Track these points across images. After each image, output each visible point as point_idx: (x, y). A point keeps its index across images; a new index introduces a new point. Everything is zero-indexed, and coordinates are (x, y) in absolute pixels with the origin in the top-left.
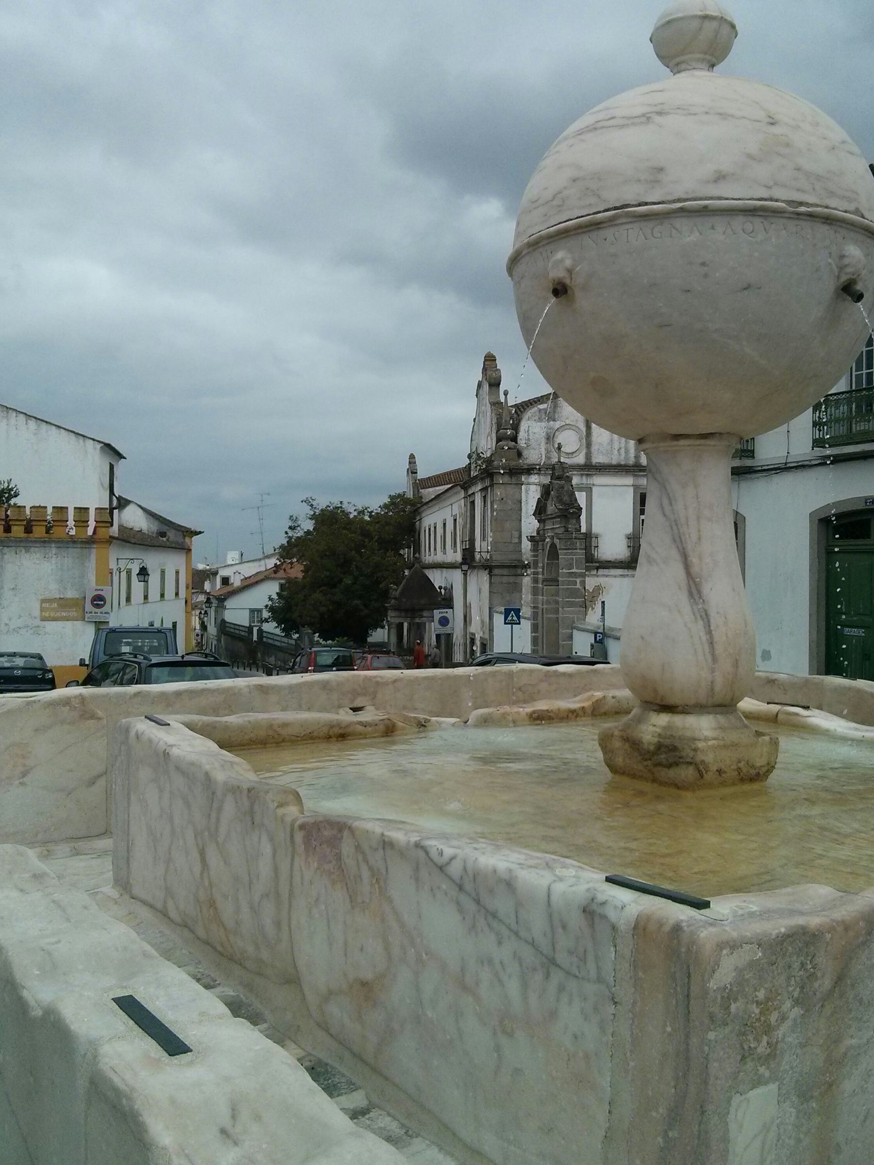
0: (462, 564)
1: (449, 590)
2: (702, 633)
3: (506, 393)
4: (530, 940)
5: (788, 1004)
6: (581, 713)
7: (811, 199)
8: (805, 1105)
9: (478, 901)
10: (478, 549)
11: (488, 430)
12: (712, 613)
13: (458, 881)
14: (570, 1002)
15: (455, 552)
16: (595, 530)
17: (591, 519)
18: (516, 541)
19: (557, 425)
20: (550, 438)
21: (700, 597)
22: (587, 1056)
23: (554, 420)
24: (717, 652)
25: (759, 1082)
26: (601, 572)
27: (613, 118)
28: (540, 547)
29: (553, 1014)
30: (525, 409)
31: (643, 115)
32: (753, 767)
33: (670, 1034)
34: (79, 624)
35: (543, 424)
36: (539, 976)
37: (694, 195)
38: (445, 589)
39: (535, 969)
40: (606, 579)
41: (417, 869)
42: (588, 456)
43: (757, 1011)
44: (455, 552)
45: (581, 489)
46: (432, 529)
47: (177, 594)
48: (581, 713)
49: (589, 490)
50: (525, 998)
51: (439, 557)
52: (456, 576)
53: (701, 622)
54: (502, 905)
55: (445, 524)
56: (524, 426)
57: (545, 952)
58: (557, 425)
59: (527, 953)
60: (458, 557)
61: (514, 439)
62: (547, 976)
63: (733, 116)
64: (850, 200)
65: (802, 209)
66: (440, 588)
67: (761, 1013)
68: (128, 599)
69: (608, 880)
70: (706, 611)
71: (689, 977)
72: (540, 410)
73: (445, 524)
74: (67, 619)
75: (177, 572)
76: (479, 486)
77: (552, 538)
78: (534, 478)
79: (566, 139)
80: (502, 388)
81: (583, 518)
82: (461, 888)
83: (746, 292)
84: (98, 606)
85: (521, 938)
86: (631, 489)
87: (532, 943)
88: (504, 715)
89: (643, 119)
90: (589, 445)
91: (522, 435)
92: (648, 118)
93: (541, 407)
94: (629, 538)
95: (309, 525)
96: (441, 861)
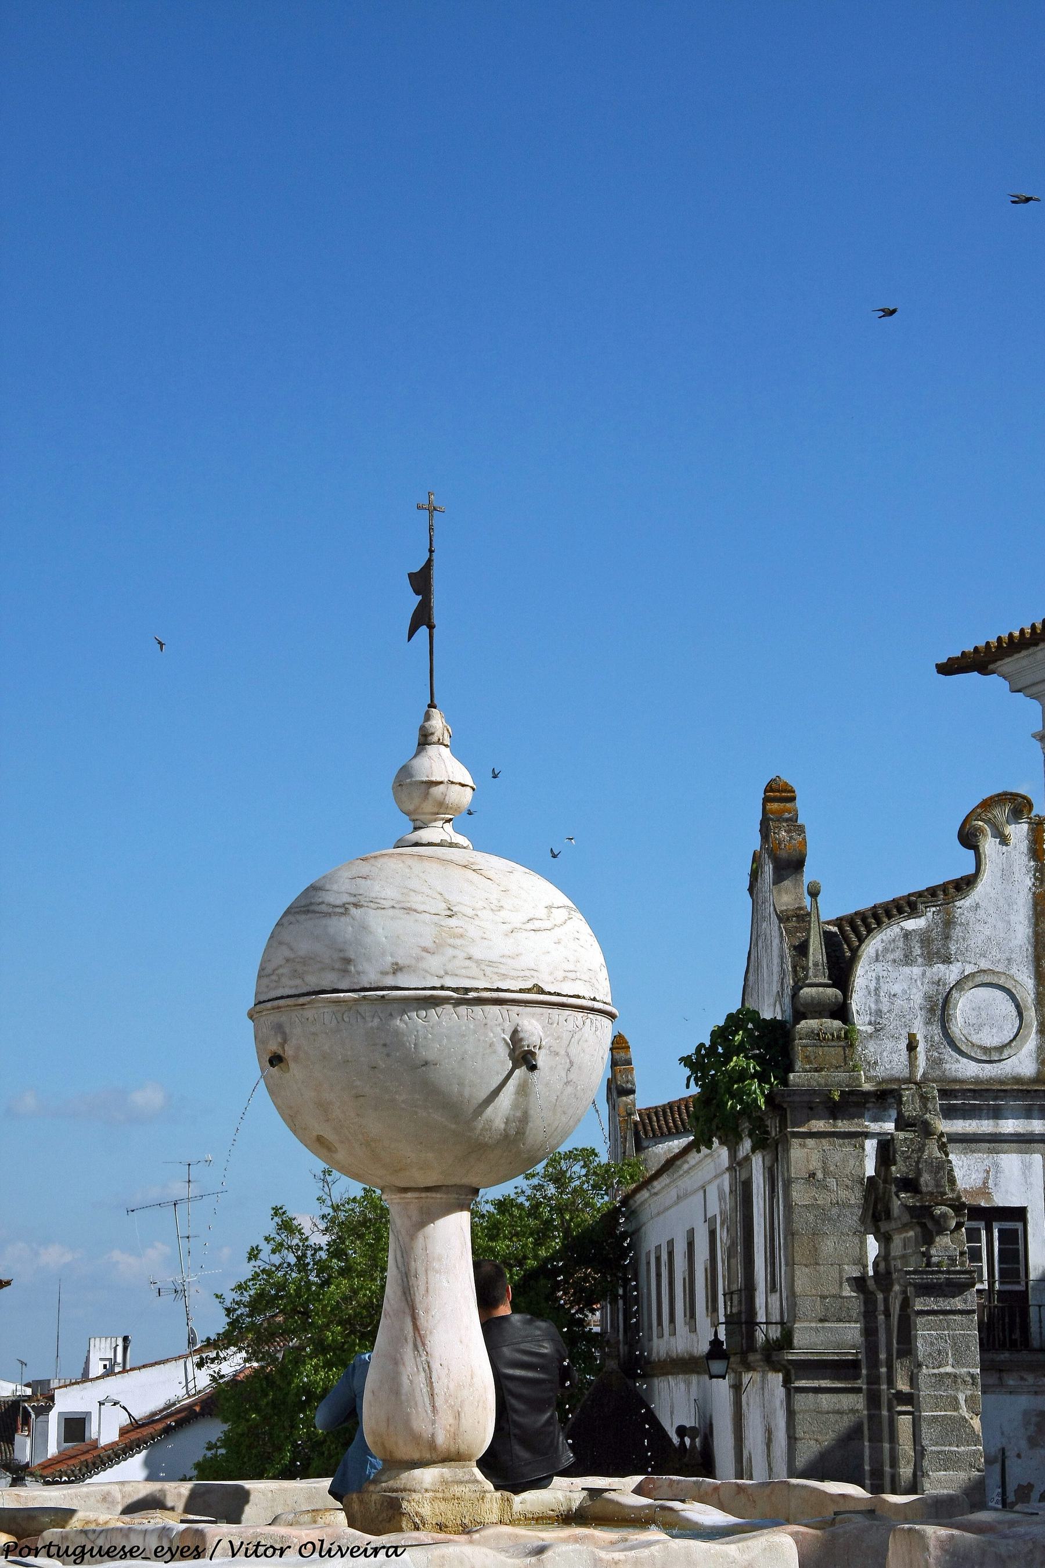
1: (706, 1432)
3: (814, 893)
7: (481, 985)
17: (710, 1241)
19: (952, 973)
21: (424, 1349)
23: (947, 960)
30: (870, 931)
35: (916, 971)
37: (376, 985)
46: (664, 1257)
53: (423, 1374)
56: (863, 976)
58: (952, 973)
61: (841, 1012)
63: (415, 911)
64: (525, 978)
65: (472, 995)
66: (681, 1431)
70: (428, 1363)
72: (907, 935)
80: (809, 874)
89: (342, 910)
91: (858, 1002)
93: (911, 924)
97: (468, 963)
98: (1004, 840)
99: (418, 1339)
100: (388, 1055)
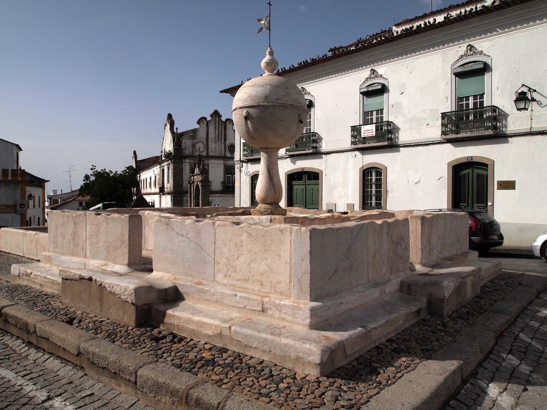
3: (177, 129)
10: (166, 186)
11: (170, 142)
15: (156, 188)
19: (196, 141)
20: (193, 146)
34: (14, 215)
42: (207, 153)
44: (156, 188)
47: (39, 206)
49: (208, 166)
51: (149, 191)
52: (157, 197)
56: (184, 141)
58: (196, 141)
60: (157, 190)
68: (34, 206)
74: (9, 213)
75: (39, 197)
76: (166, 163)
77: (484, 334)
78: (188, 161)
84: (22, 208)
90: (208, 149)
95: (93, 178)
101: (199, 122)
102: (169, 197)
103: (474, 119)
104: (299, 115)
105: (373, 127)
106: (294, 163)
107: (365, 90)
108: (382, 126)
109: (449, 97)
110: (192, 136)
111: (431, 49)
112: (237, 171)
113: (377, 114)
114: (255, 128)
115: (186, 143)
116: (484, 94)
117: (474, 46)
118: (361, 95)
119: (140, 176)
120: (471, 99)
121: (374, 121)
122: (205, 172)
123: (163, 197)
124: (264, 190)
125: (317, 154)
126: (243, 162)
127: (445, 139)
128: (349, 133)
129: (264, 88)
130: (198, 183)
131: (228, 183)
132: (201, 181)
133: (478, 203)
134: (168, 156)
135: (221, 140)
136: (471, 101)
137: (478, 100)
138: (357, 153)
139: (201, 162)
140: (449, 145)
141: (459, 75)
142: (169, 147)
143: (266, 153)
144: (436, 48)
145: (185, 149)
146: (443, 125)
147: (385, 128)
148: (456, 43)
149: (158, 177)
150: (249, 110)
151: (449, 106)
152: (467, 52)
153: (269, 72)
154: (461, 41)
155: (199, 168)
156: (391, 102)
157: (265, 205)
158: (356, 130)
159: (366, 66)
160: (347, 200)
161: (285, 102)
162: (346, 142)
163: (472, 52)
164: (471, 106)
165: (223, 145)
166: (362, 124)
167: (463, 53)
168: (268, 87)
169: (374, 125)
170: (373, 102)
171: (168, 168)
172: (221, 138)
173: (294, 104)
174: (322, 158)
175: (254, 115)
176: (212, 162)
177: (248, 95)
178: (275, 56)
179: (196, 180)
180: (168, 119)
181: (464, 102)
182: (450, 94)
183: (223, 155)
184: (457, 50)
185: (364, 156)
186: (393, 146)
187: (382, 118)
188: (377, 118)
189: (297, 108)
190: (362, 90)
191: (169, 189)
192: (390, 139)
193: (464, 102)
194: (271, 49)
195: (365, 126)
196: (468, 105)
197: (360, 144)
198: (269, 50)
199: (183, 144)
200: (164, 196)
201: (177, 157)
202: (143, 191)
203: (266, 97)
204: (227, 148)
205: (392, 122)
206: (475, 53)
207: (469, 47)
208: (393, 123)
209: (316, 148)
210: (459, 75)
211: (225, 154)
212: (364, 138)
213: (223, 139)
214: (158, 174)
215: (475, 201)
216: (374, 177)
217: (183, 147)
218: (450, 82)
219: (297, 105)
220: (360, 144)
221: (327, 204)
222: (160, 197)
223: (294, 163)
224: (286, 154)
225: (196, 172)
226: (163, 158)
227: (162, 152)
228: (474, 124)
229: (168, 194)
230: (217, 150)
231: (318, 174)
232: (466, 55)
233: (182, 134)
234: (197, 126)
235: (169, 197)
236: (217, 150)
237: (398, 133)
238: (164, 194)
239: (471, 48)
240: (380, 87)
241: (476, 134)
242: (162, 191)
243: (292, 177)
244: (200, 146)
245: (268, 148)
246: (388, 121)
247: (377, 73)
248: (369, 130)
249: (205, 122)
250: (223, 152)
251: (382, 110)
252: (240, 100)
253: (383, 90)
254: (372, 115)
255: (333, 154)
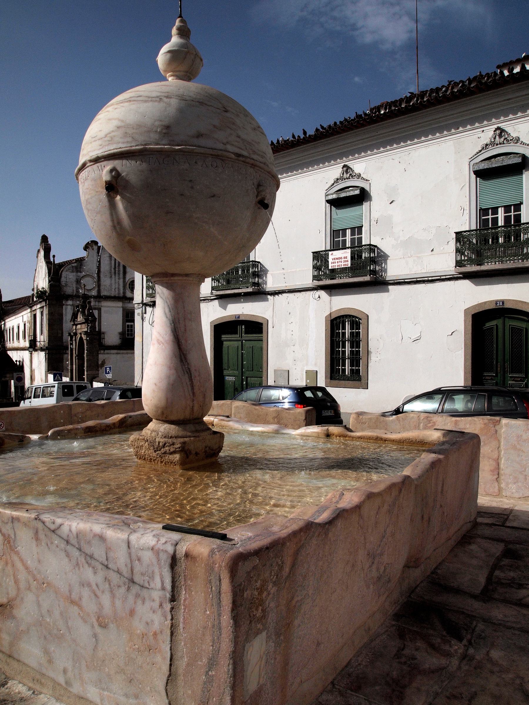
0: (29, 348)
2: (188, 380)
3: (54, 256)
4: (116, 570)
5: (271, 585)
6: (113, 427)
8: (278, 639)
9: (80, 549)
10: (38, 339)
11: (44, 276)
12: (193, 371)
13: (66, 538)
14: (143, 603)
15: (25, 341)
16: (103, 330)
18: (60, 335)
20: (78, 282)
21: (186, 361)
22: (155, 634)
23: (81, 272)
24: (195, 391)
25: (258, 633)
26: (106, 351)
27: (140, 96)
28: (74, 339)
29: (132, 613)
31: (157, 97)
32: (212, 450)
33: (209, 615)
35: (74, 274)
36: (123, 590)
38: (19, 361)
39: (119, 586)
40: (109, 355)
41: (37, 532)
42: (99, 291)
43: (257, 593)
44: (25, 341)
45: (95, 309)
48: (113, 427)
49: (99, 310)
50: (113, 603)
51: (16, 344)
53: (187, 375)
54: (98, 552)
55: (18, 327)
56: (64, 274)
57: (126, 576)
59: (114, 577)
60: (27, 344)
62: (129, 589)
63: (206, 104)
67: (258, 594)
69: (164, 528)
70: (189, 369)
71: (220, 580)
72: (73, 267)
73: (18, 327)
76: (39, 306)
78: (70, 302)
79: (112, 105)
81: (97, 323)
82: (68, 542)
83: (212, 199)
85: (109, 569)
86: (121, 309)
87: (118, 572)
88: (69, 431)
90: (99, 286)
92: (161, 99)
94: (120, 334)
96: (53, 527)
97: (238, 139)
98: (93, 249)
99: (183, 356)
100: (192, 188)
101: (86, 248)
102: (42, 354)
103: (505, 242)
104: (259, 185)
105: (347, 254)
106: (225, 308)
107: (334, 196)
108: (361, 252)
109: (467, 208)
110: (76, 267)
111: (438, 135)
112: (137, 319)
113: (353, 234)
114: (134, 218)
115: (68, 277)
116: (521, 203)
117: (506, 129)
118: (328, 205)
119: (4, 324)
120: (501, 211)
121: (348, 244)
122: (91, 320)
123: (35, 354)
124: (163, 385)
125: (259, 294)
126: (146, 305)
127: (460, 273)
128: (309, 262)
129: (162, 105)
130: (83, 336)
131: (128, 335)
132: (86, 333)
133: (512, 372)
134: (41, 295)
135: (119, 274)
136: (501, 215)
137: (512, 214)
138: (322, 293)
139: (87, 306)
140: (466, 283)
141: (483, 174)
142: (42, 282)
143: (169, 286)
144: (445, 133)
145: (66, 285)
146: (458, 251)
147: (365, 255)
148: (477, 125)
149: (27, 325)
150: (117, 164)
151: (466, 222)
152: (495, 138)
153: (179, 78)
154: (485, 122)
155: (83, 313)
156: (375, 215)
157: (166, 426)
158: (320, 258)
159: (335, 160)
160: (307, 365)
161: (220, 146)
162: (305, 276)
163: (502, 139)
164: (501, 222)
165: (121, 281)
166: (328, 248)
167: (488, 141)
168: (174, 102)
169: (349, 251)
170: (346, 216)
171: (41, 312)
172: (119, 271)
173: (245, 153)
174: (267, 300)
175: (133, 179)
176: (105, 305)
177: (116, 123)
178: (193, 40)
179: (79, 331)
180: (41, 243)
181: (490, 217)
182: (468, 203)
183: (121, 295)
184: (479, 136)
185: (333, 297)
186: (379, 284)
187: (360, 239)
188: (353, 241)
189: (253, 166)
190: (330, 197)
191: (42, 343)
192: (373, 272)
193: (490, 217)
194: (182, 21)
195: (334, 252)
196: (495, 220)
197: (327, 280)
198: (178, 23)
199: (63, 279)
200: (36, 353)
201: (54, 297)
202: (9, 345)
203: (168, 127)
204: (128, 286)
205: (376, 246)
206: (508, 141)
207: (498, 132)
208: (378, 248)
209: (374, 272)
210: (483, 174)
211: (124, 293)
212: (333, 271)
213: (121, 272)
214: (29, 322)
215: (508, 369)
216: (348, 330)
217: (63, 283)
218: (467, 185)
219: (255, 157)
220: (327, 280)
221: (275, 371)
222: (31, 354)
223: (225, 308)
224: (212, 293)
225: (79, 319)
226: (35, 299)
227: (33, 290)
228: (505, 251)
229: (42, 349)
230: (113, 287)
231: (262, 324)
232: (493, 144)
233: (61, 265)
234: (84, 254)
235: (42, 354)
236: (113, 287)
237: (386, 263)
238: (36, 350)
239: (501, 133)
240: (357, 192)
241: (509, 265)
242: (33, 346)
243: (222, 329)
244: (89, 283)
245: (173, 275)
246: (370, 245)
247: (353, 171)
248: (340, 259)
249: (95, 248)
250: (122, 291)
251: (360, 228)
252: (94, 138)
253: (362, 197)
254: (344, 235)
255: (285, 295)
